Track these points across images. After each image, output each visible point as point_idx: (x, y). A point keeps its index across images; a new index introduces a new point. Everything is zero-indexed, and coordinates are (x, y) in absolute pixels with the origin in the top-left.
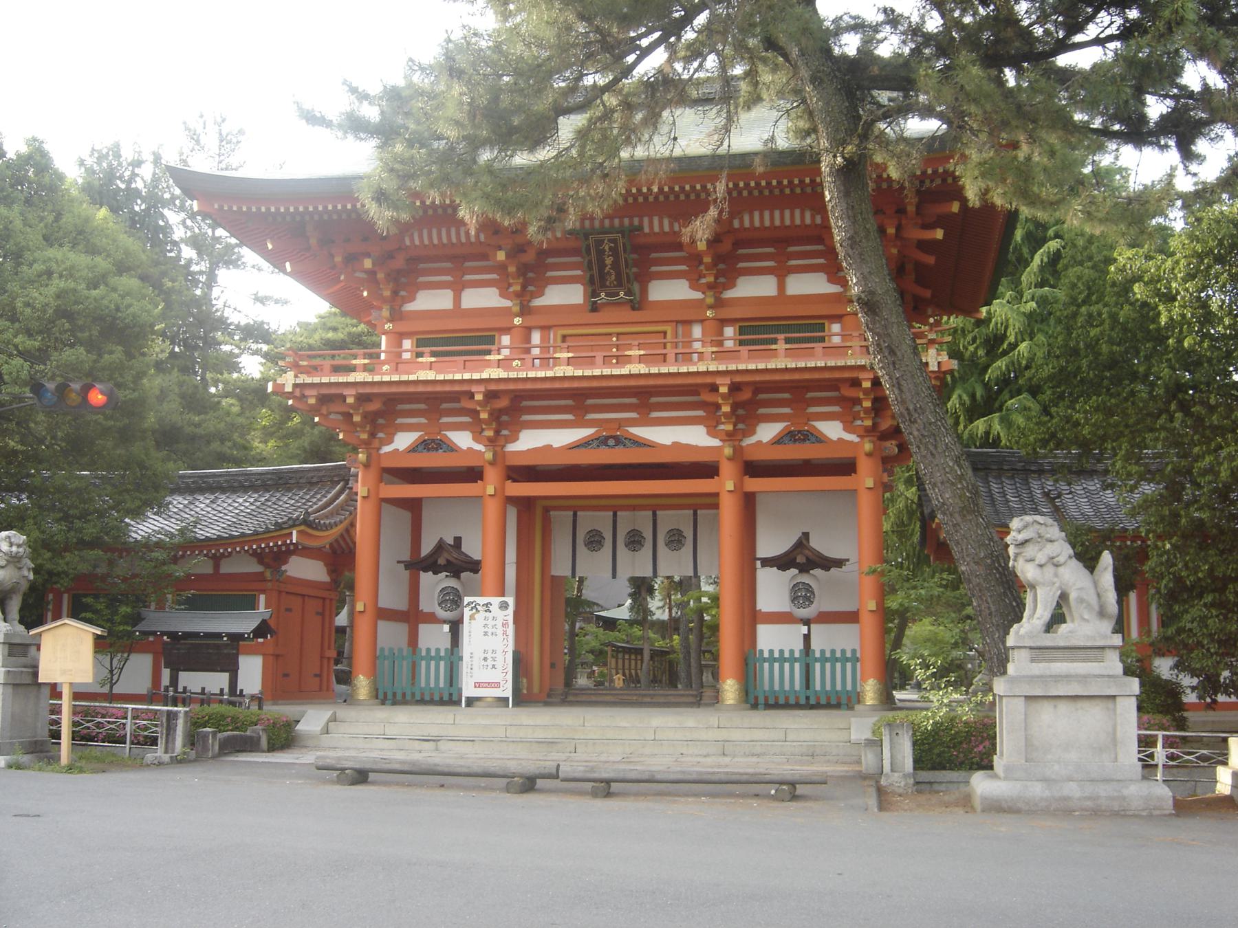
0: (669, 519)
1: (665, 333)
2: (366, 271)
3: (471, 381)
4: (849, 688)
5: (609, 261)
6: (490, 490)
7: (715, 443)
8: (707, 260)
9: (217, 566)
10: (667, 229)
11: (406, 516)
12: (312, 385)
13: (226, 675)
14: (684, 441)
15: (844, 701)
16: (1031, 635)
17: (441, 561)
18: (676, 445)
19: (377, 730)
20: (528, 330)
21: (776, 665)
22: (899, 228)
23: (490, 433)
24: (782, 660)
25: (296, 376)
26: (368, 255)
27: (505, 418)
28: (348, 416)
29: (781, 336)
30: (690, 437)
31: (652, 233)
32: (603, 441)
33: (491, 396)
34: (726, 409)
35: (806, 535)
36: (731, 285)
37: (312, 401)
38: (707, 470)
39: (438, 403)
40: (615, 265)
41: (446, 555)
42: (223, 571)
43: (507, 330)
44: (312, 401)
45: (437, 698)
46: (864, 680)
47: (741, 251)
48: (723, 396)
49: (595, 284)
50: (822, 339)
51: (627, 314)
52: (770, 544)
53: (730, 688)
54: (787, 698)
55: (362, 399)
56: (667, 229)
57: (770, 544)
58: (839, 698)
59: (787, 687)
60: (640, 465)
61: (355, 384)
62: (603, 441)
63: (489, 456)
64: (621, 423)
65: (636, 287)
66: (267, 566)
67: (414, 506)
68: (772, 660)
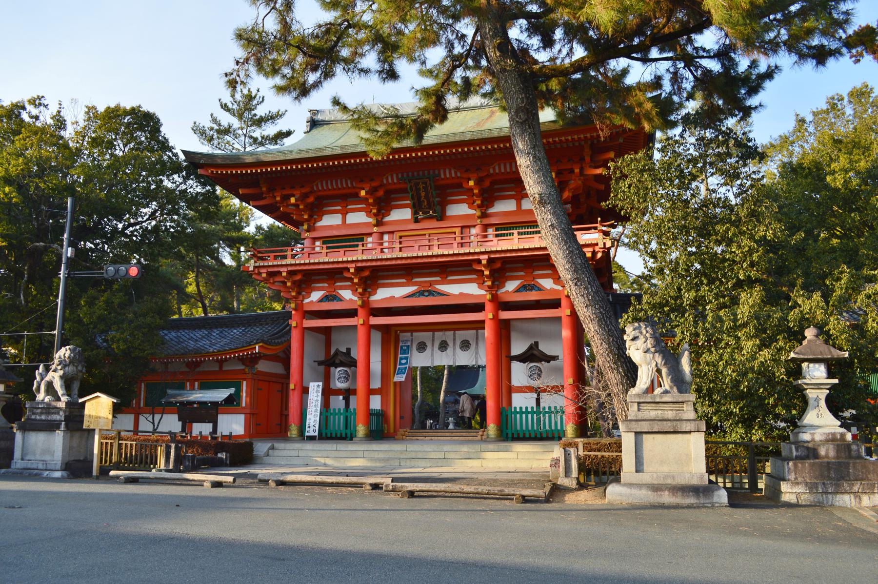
0: (462, 335)
1: (455, 233)
2: (293, 205)
3: (348, 262)
4: (559, 428)
5: (423, 194)
6: (361, 322)
7: (483, 292)
8: (476, 191)
9: (221, 367)
10: (453, 175)
11: (323, 337)
12: (264, 267)
13: (211, 425)
14: (466, 292)
15: (556, 435)
16: (638, 395)
17: (337, 361)
18: (461, 294)
19: (295, 453)
20: (382, 234)
21: (524, 416)
22: (582, 169)
23: (360, 290)
24: (527, 413)
25: (255, 262)
26: (293, 196)
27: (369, 282)
28: (284, 283)
29: (515, 232)
30: (469, 289)
31: (446, 178)
32: (421, 293)
33: (359, 270)
34: (487, 273)
35: (537, 343)
36: (491, 205)
37: (264, 275)
38: (478, 307)
39: (334, 275)
40: (426, 196)
41: (339, 357)
42: (225, 368)
43: (370, 234)
44: (264, 275)
45: (533, 436)
46: (567, 423)
47: (496, 187)
48: (484, 266)
49: (416, 210)
50: (539, 232)
51: (434, 224)
52: (518, 347)
53: (294, 431)
54: (524, 434)
55: (291, 273)
56: (453, 175)
57: (518, 347)
58: (553, 434)
59: (524, 428)
60: (447, 306)
61: (286, 265)
62: (421, 293)
63: (360, 303)
64: (431, 284)
65: (438, 208)
66: (246, 366)
67: (327, 331)
68: (521, 413)
